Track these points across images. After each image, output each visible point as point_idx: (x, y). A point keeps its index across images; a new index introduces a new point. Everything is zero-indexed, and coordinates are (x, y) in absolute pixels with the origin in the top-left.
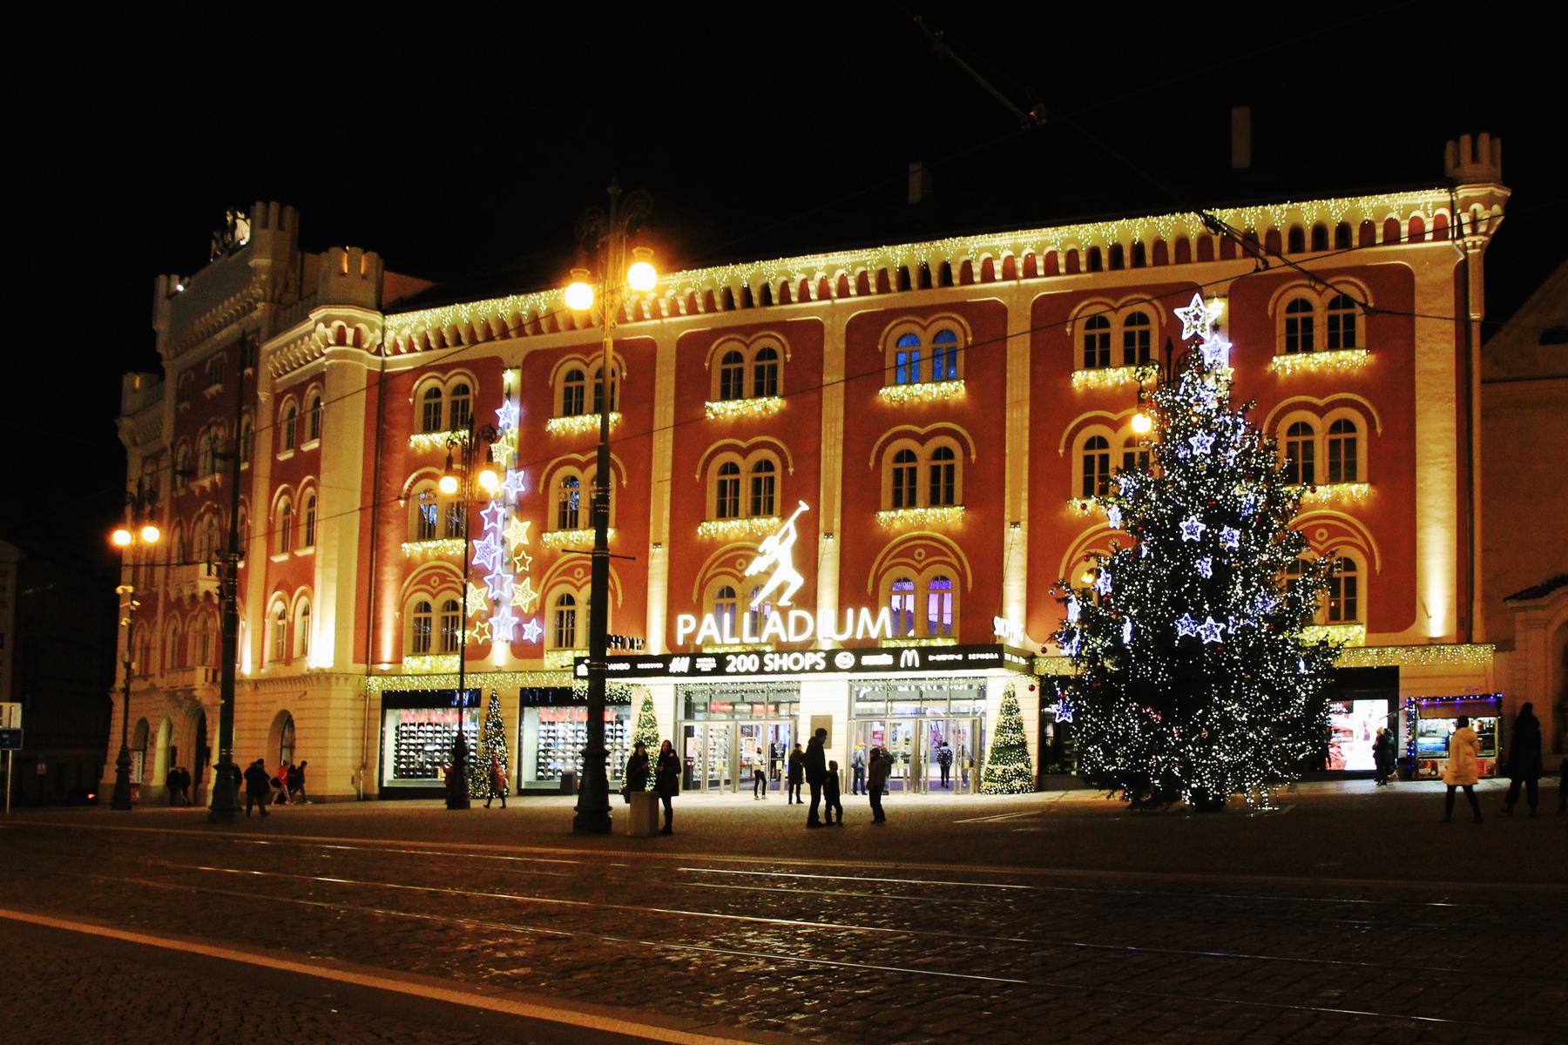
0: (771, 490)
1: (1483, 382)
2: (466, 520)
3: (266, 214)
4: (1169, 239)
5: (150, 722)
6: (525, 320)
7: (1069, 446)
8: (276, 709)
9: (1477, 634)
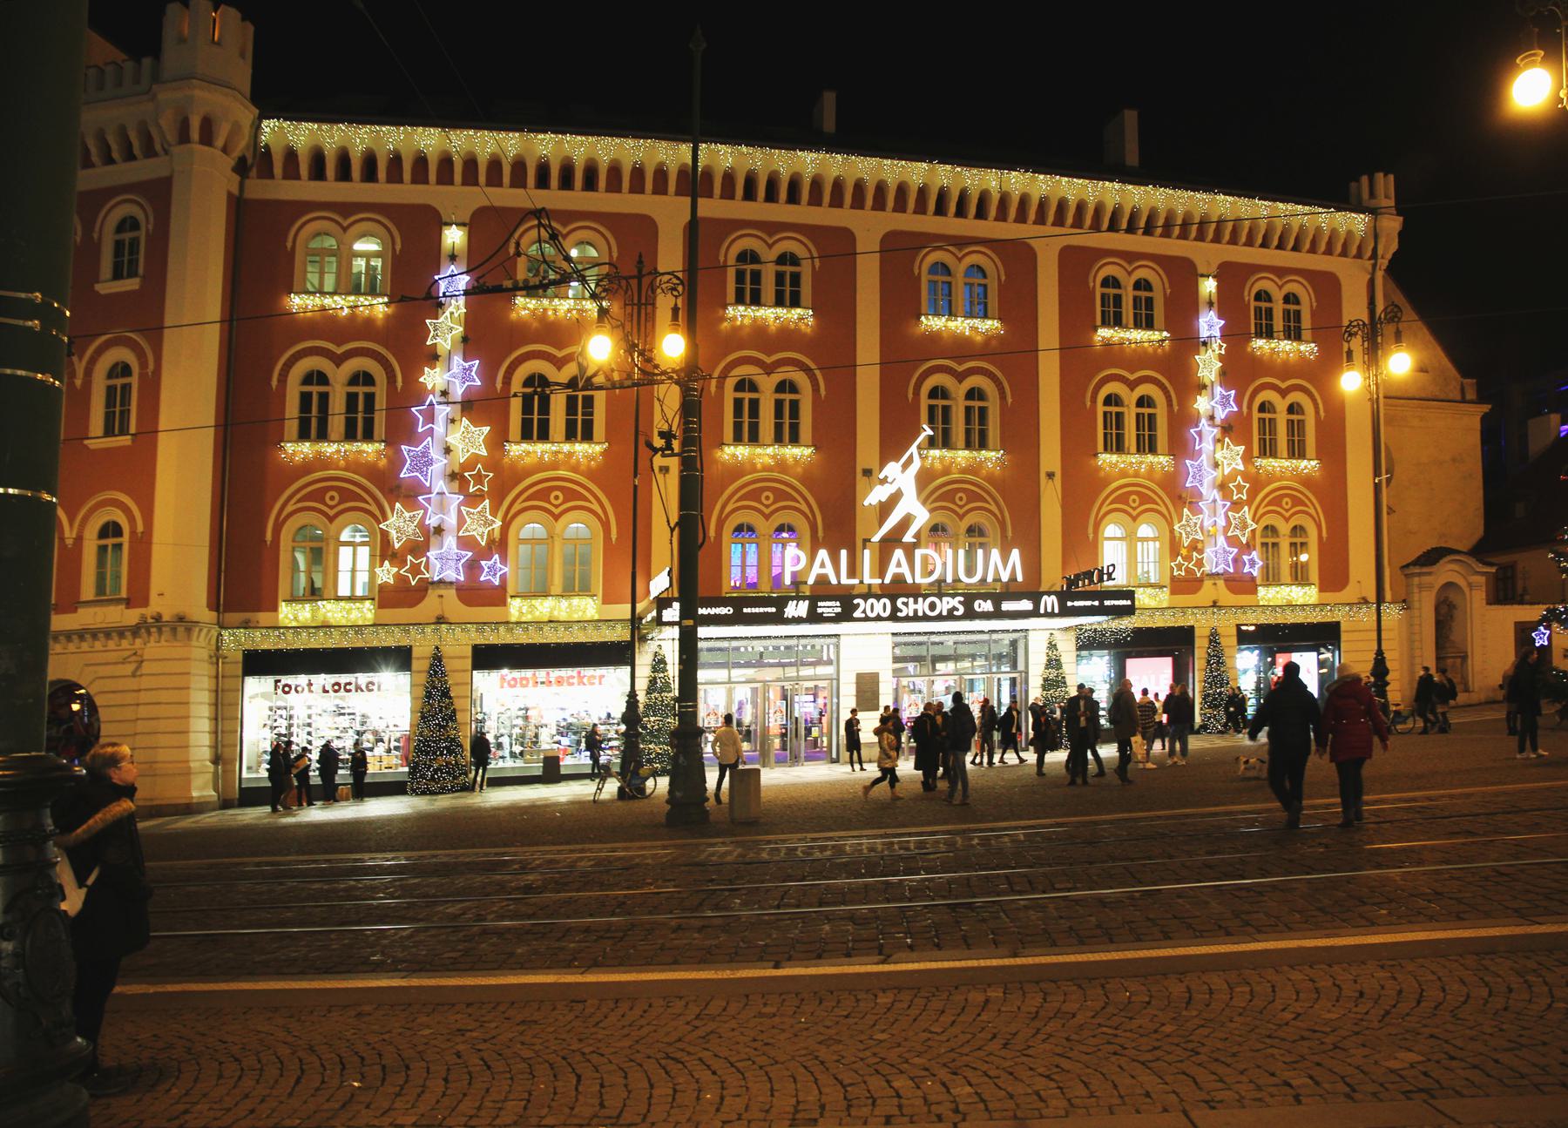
6: (807, 181)
7: (89, 372)
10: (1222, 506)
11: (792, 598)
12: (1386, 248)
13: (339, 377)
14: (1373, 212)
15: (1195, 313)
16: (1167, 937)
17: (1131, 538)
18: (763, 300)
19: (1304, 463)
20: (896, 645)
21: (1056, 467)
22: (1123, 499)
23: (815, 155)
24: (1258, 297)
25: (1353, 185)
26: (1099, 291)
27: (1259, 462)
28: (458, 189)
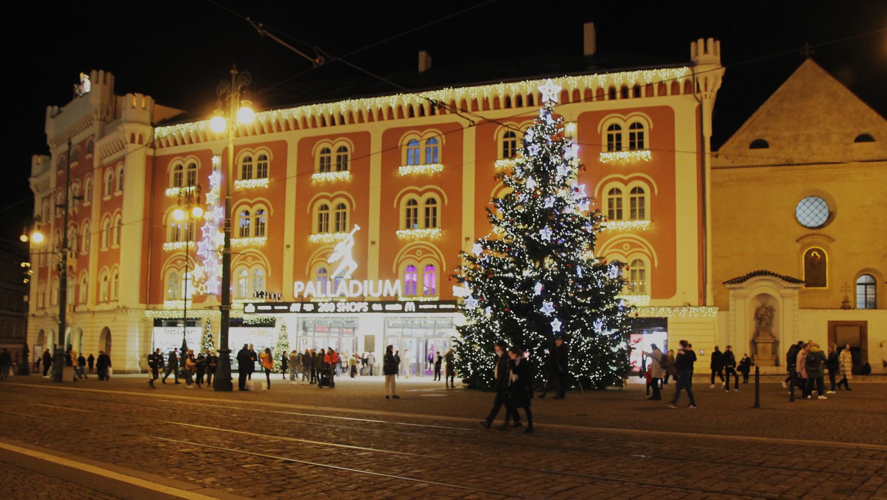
0: (345, 219)
1: (713, 168)
2: (193, 233)
3: (98, 76)
4: (355, 110)
5: (45, 331)
7: (311, 209)
8: (103, 327)
9: (710, 300)
13: (421, 201)
28: (293, 132)
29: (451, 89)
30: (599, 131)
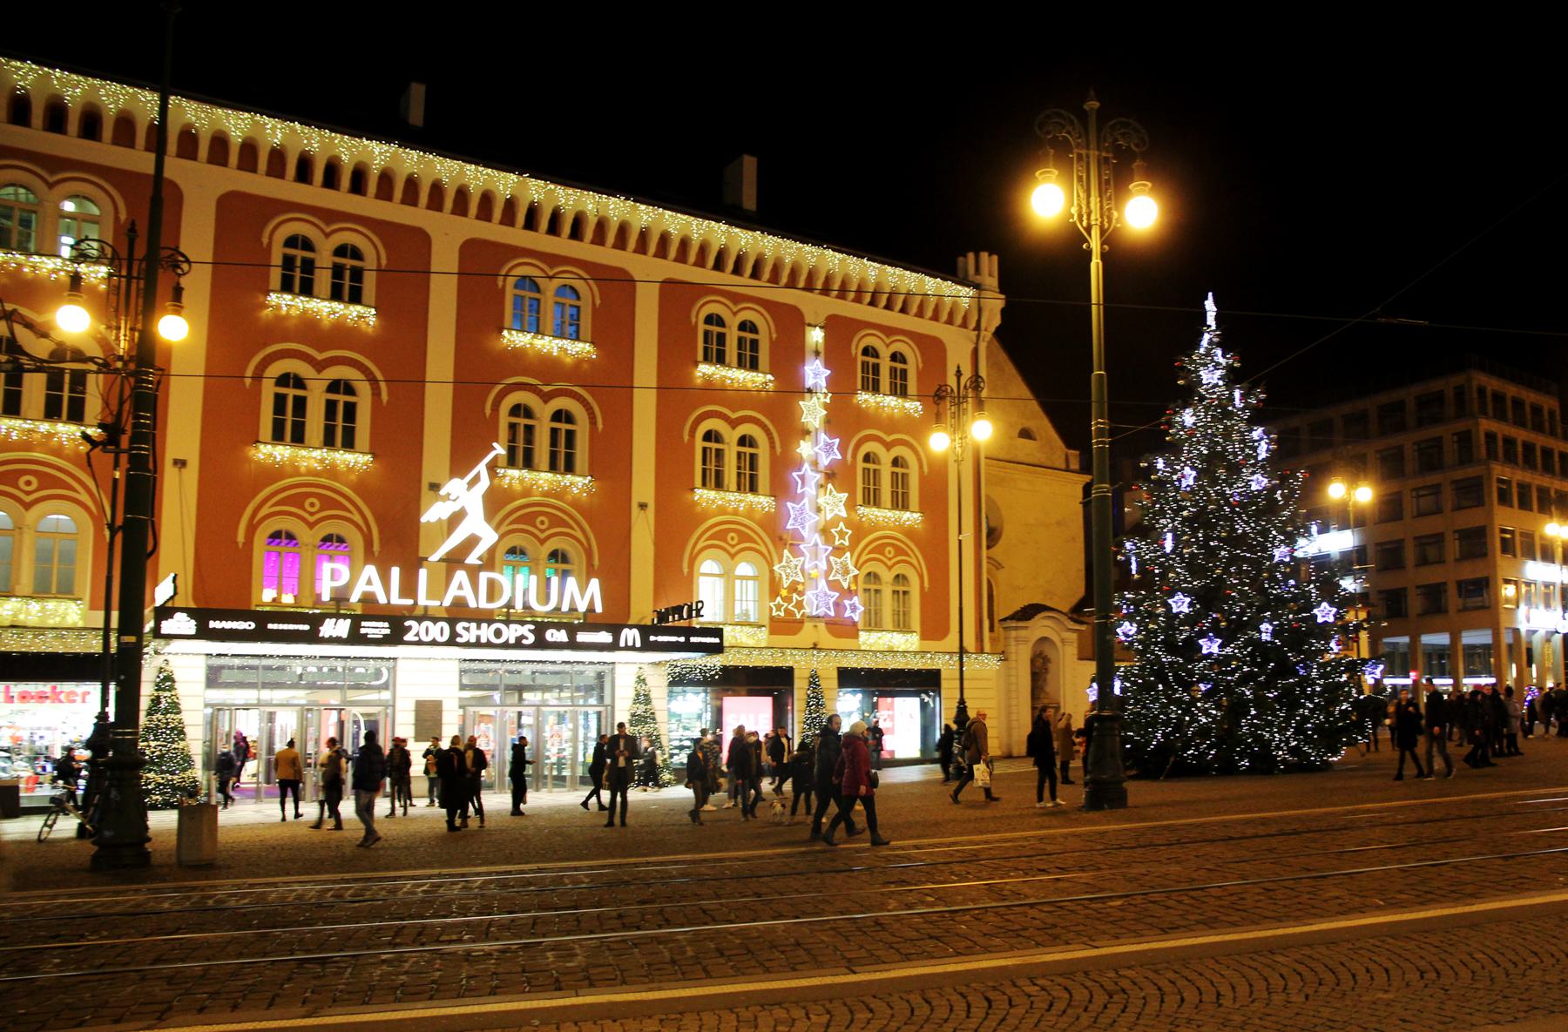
4: (696, 238)
7: (258, 377)
9: (987, 647)
10: (824, 550)
11: (330, 616)
12: (990, 320)
14: (977, 286)
15: (801, 359)
16: (876, 961)
17: (728, 576)
18: (316, 289)
19: (906, 515)
20: (463, 672)
21: (650, 500)
22: (721, 536)
23: (385, 147)
24: (866, 351)
25: (961, 259)
26: (702, 327)
27: (862, 510)
29: (630, 203)
30: (265, 240)
